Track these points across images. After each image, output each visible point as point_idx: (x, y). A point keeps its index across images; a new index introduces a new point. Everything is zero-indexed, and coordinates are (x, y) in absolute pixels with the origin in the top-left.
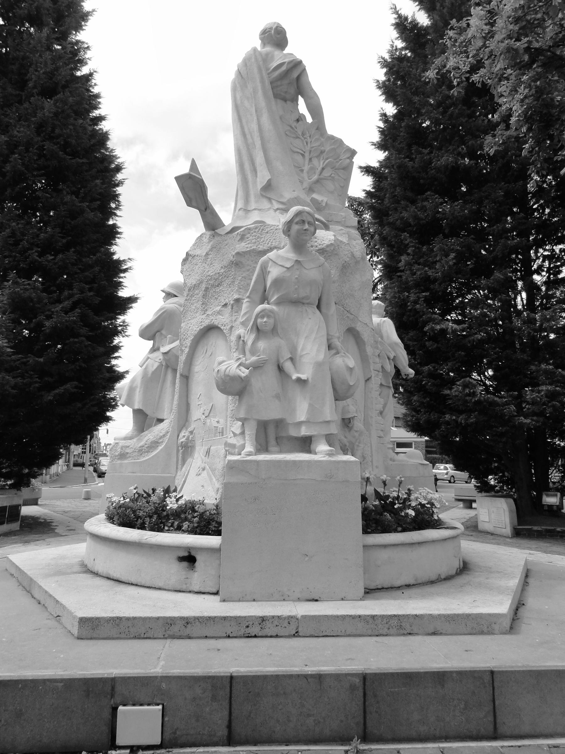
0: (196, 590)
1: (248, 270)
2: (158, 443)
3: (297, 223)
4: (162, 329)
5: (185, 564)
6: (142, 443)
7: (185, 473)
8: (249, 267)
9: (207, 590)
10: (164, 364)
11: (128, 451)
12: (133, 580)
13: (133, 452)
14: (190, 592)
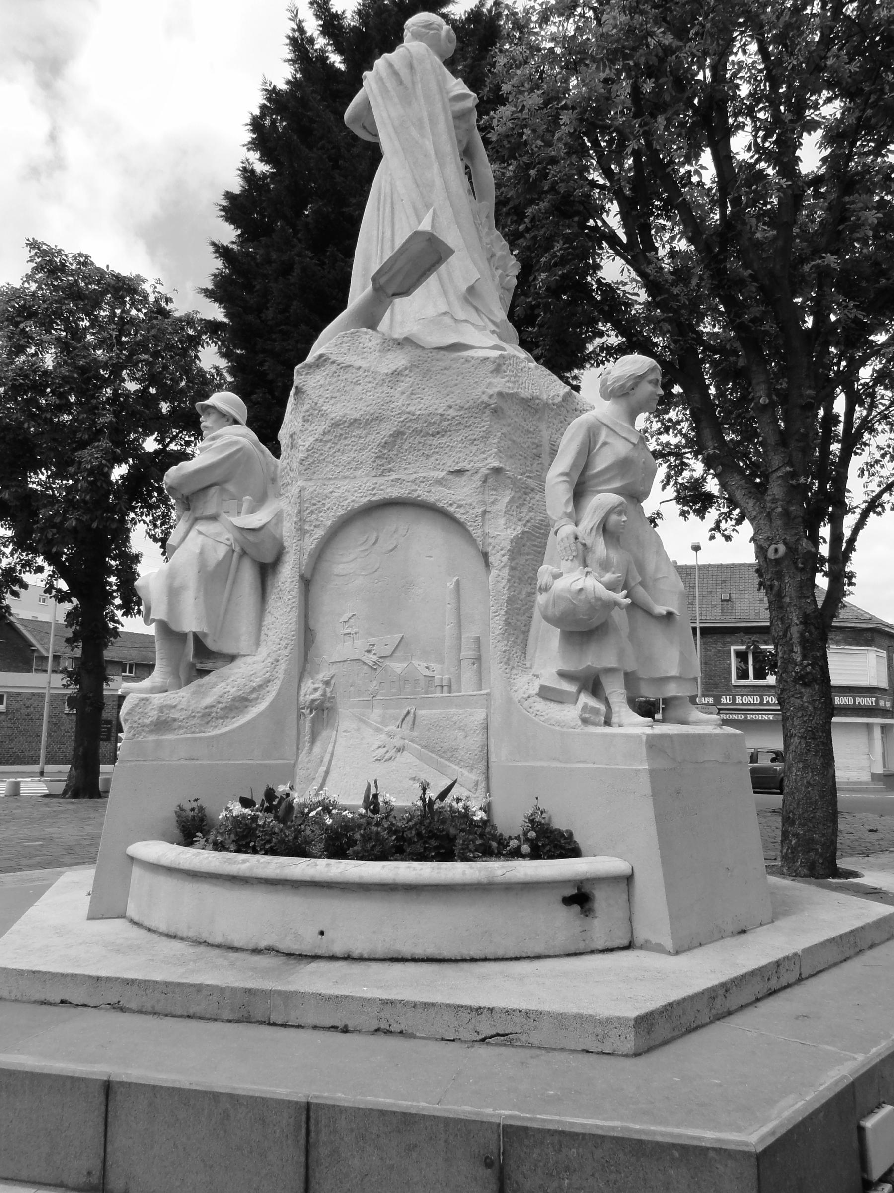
0: (600, 948)
1: (509, 425)
2: (246, 700)
3: (650, 382)
4: (226, 481)
5: (576, 908)
6: (208, 701)
7: (322, 757)
8: (509, 420)
9: (616, 945)
10: (238, 549)
11: (176, 716)
12: (474, 952)
13: (188, 718)
14: (592, 952)
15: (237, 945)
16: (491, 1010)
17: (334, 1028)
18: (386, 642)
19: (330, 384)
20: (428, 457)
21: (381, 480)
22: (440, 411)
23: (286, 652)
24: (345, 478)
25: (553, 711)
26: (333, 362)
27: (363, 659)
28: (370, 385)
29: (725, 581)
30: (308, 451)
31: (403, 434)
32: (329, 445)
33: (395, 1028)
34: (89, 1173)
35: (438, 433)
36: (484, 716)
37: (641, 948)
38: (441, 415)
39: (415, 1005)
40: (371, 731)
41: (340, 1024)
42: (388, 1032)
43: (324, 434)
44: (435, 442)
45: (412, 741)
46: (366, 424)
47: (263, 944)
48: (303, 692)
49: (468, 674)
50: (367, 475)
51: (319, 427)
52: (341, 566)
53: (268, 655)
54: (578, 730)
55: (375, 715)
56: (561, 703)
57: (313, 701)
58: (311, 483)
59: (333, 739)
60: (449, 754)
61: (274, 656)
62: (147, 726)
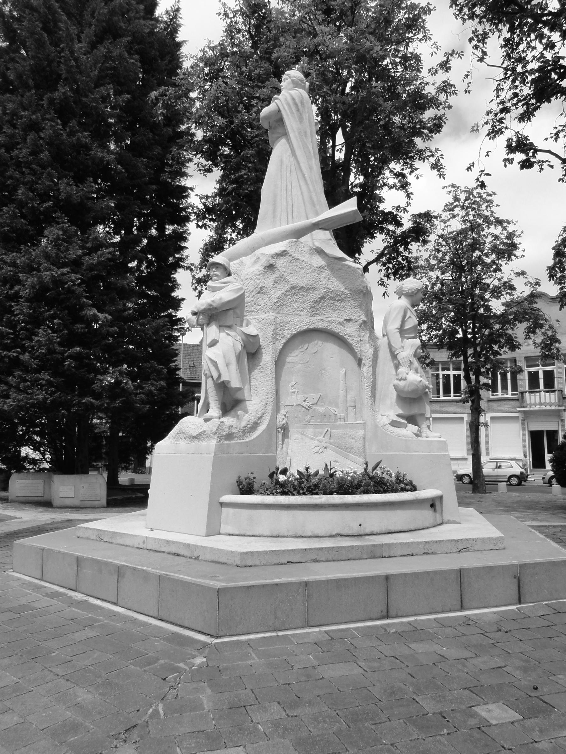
6: (244, 424)
15: (320, 535)
16: (462, 540)
17: (408, 555)
18: (313, 397)
19: (289, 266)
20: (335, 310)
21: (313, 318)
22: (342, 290)
23: (272, 400)
24: (296, 315)
25: (402, 431)
26: (290, 256)
27: (302, 404)
28: (308, 271)
29: (189, 355)
30: (278, 298)
31: (325, 298)
32: (288, 297)
33: (430, 551)
34: (382, 612)
35: (340, 300)
36: (363, 433)
37: (446, 523)
38: (342, 292)
39: (436, 542)
40: (309, 440)
41: (410, 553)
42: (428, 553)
43: (287, 291)
44: (339, 304)
45: (330, 444)
46: (307, 290)
47: (334, 533)
48: (278, 420)
49: (351, 413)
50: (306, 315)
51: (283, 288)
52: (290, 358)
53: (261, 401)
54: (414, 439)
55: (310, 432)
56: (398, 427)
57: (284, 424)
58: (280, 315)
59: (290, 443)
60: (349, 450)
61: (265, 402)
62: (224, 436)
